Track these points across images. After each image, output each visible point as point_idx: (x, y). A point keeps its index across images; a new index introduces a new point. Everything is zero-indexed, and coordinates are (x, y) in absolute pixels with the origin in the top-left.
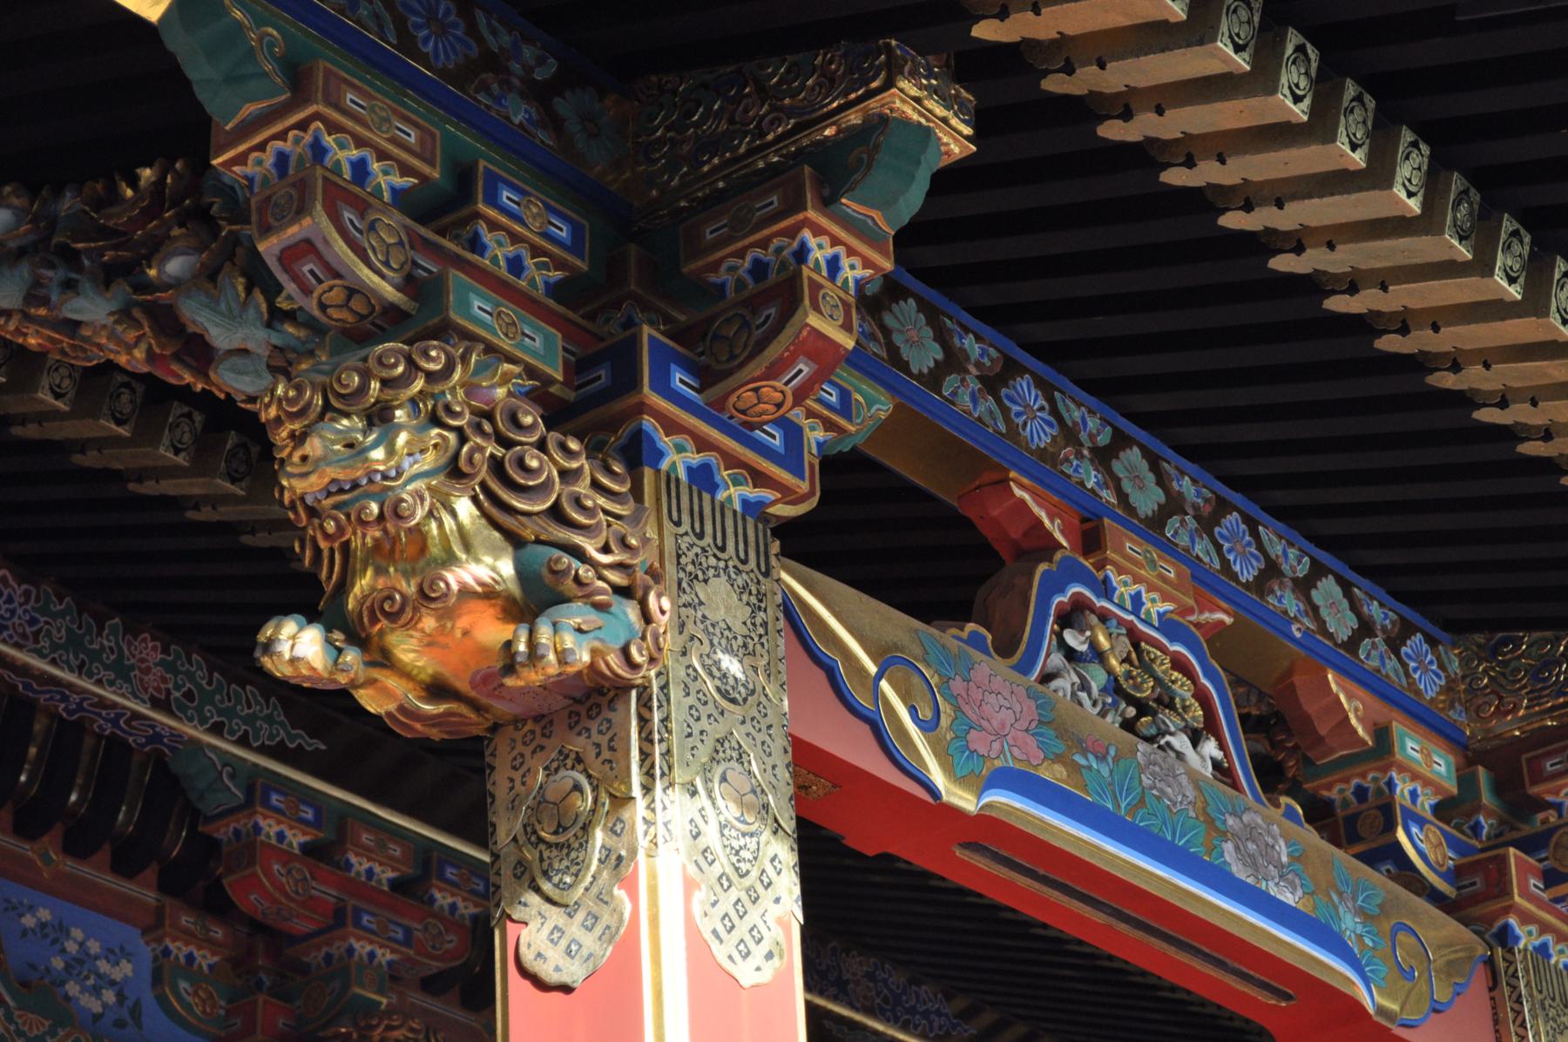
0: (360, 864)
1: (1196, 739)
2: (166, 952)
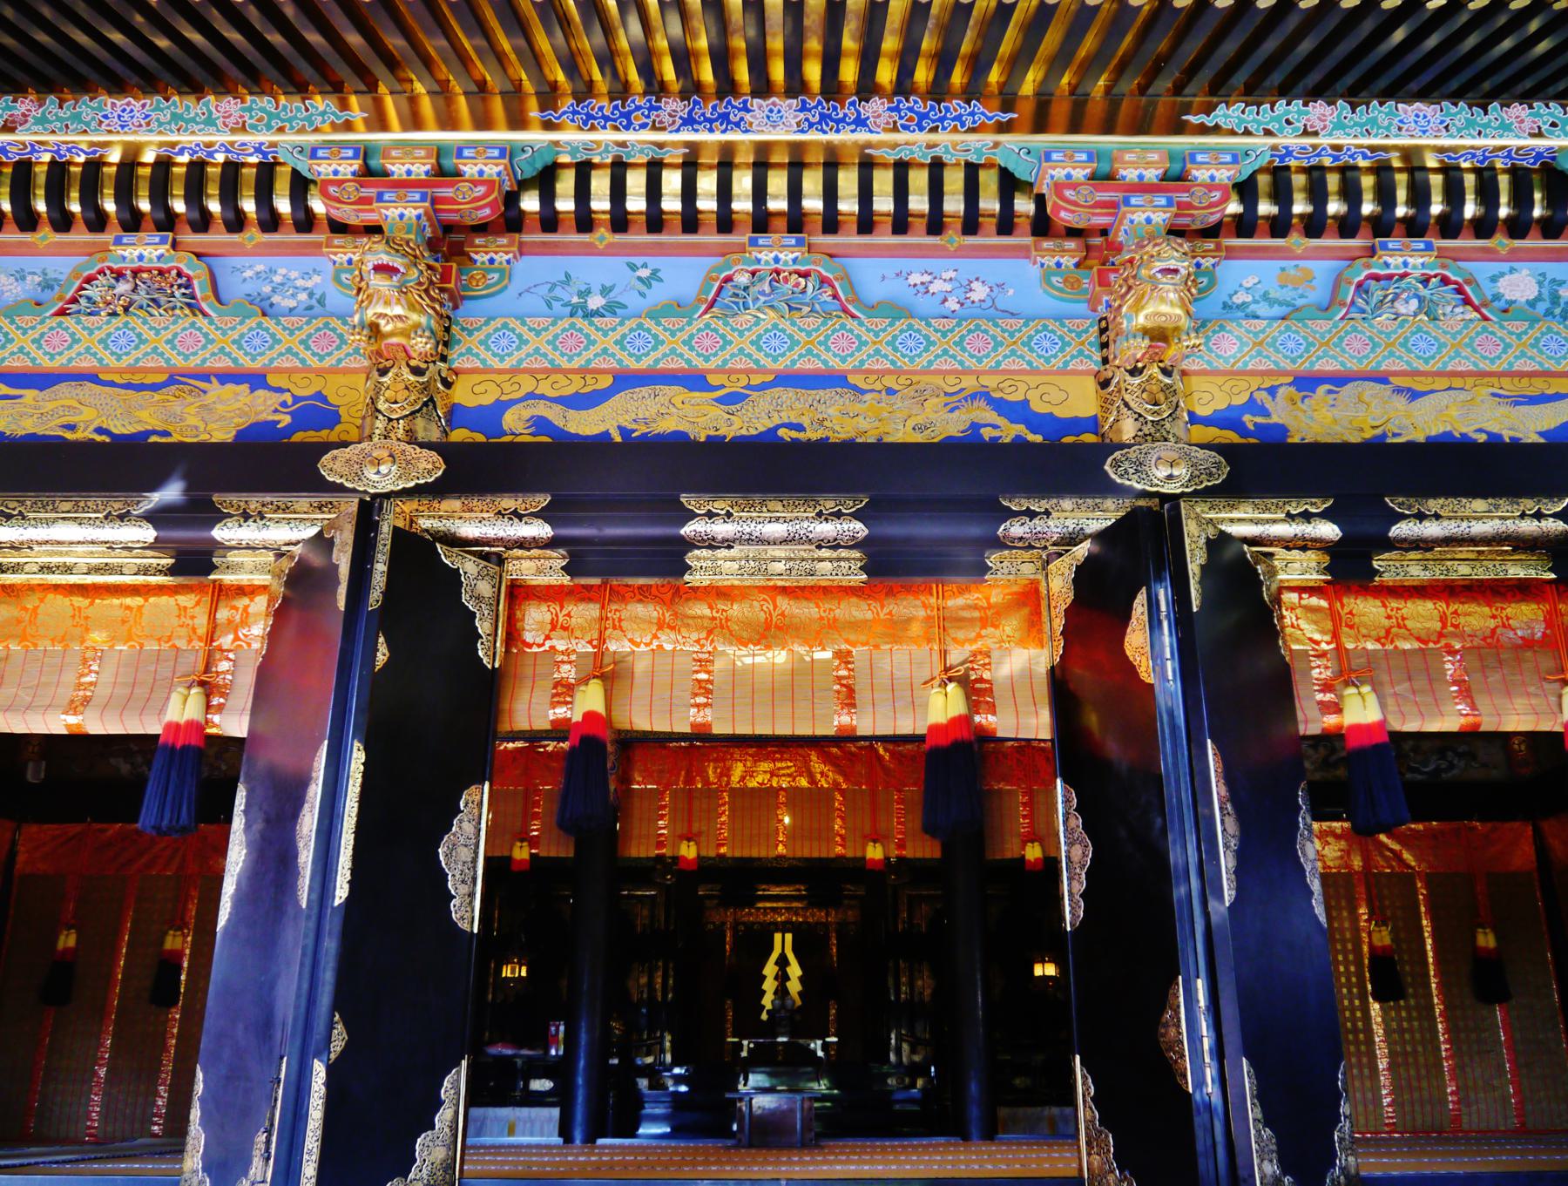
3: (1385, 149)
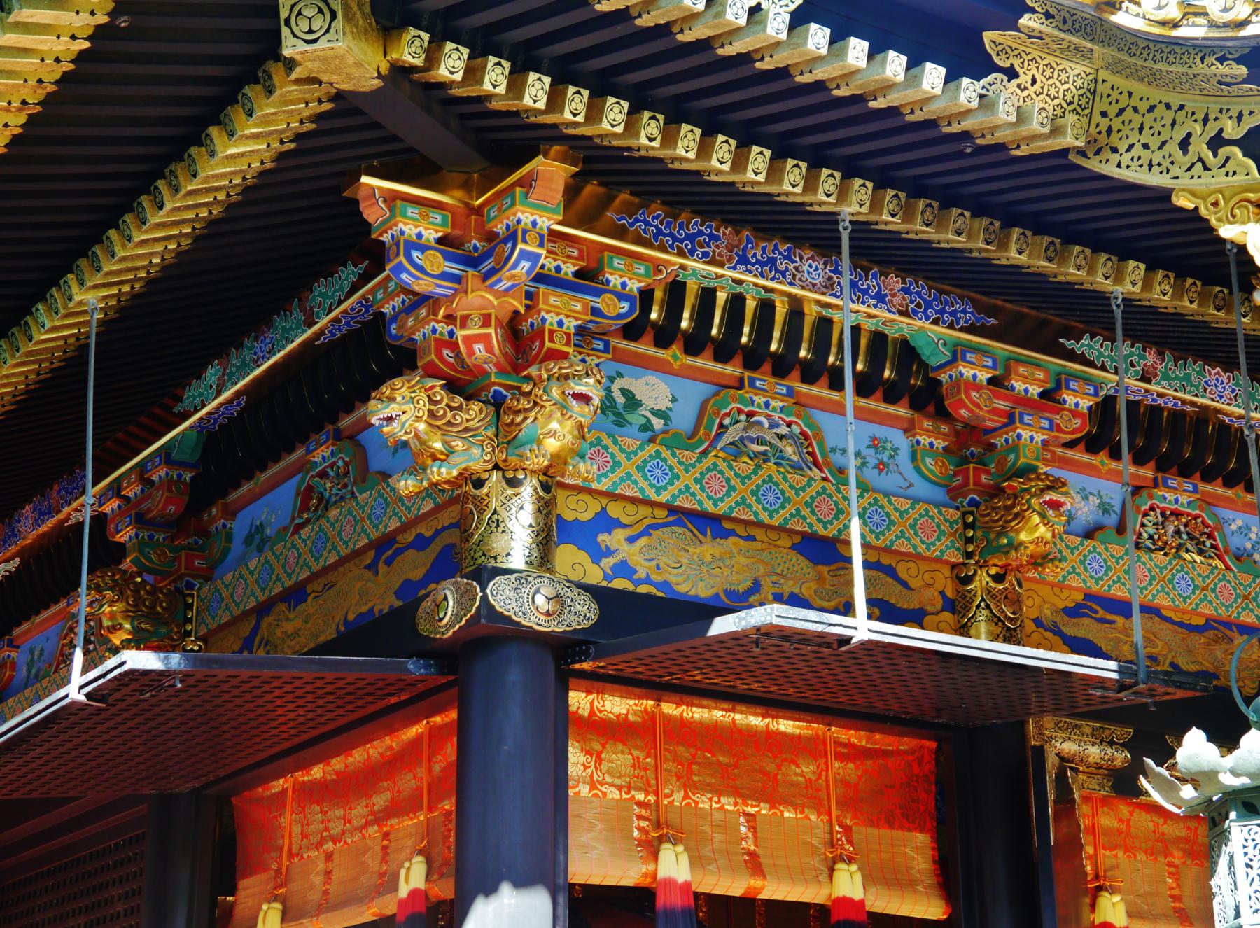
0: (1019, 386)
2: (918, 442)
3: (771, 290)
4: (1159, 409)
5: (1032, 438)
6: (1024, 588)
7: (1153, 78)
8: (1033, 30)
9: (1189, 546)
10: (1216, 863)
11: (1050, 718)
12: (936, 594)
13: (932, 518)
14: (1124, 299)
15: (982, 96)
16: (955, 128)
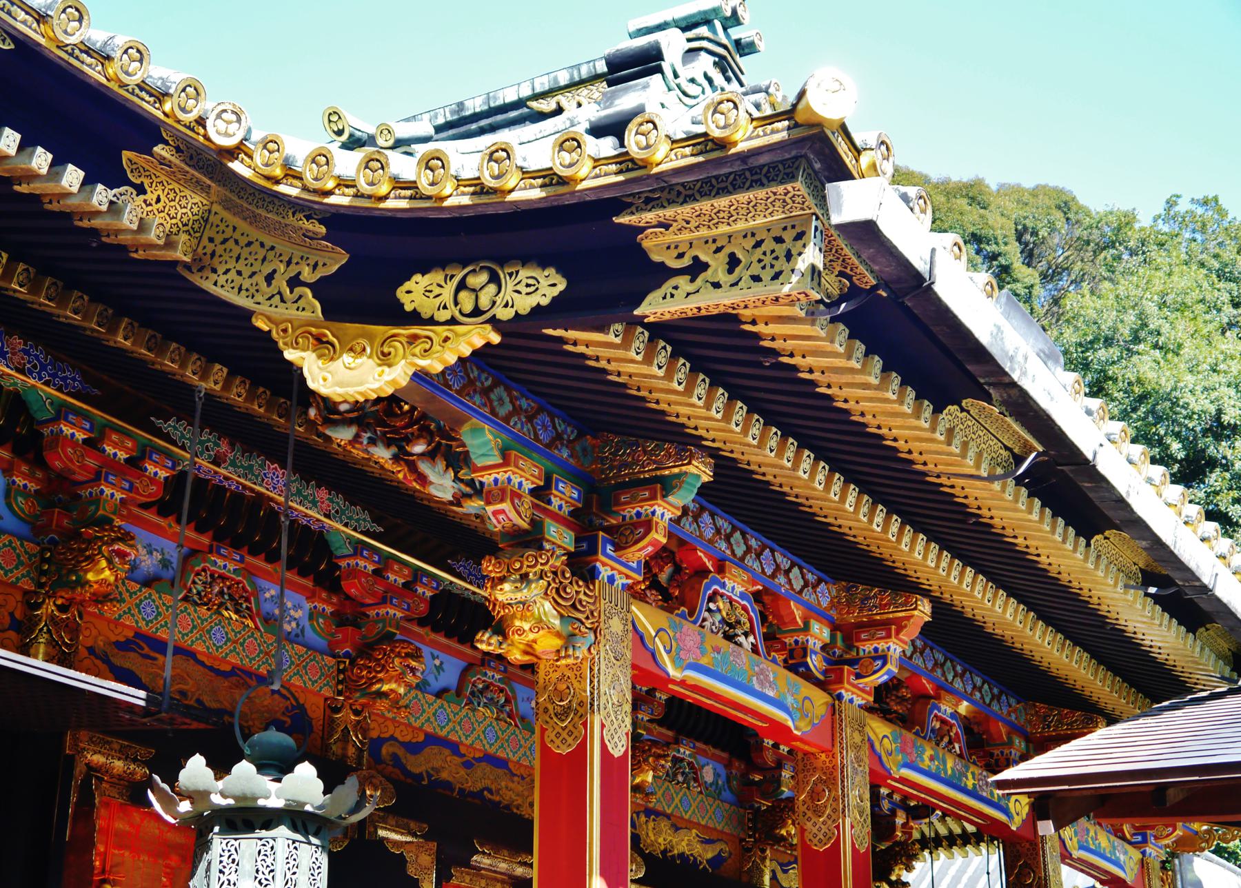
0: (392, 577)
1: (746, 635)
2: (14, 482)
4: (224, 489)
5: (112, 495)
6: (85, 620)
7: (254, 220)
8: (164, 159)
9: (229, 605)
10: (196, 868)
11: (86, 732)
12: (6, 614)
13: (14, 549)
14: (205, 394)
15: (111, 203)
16: (85, 224)
